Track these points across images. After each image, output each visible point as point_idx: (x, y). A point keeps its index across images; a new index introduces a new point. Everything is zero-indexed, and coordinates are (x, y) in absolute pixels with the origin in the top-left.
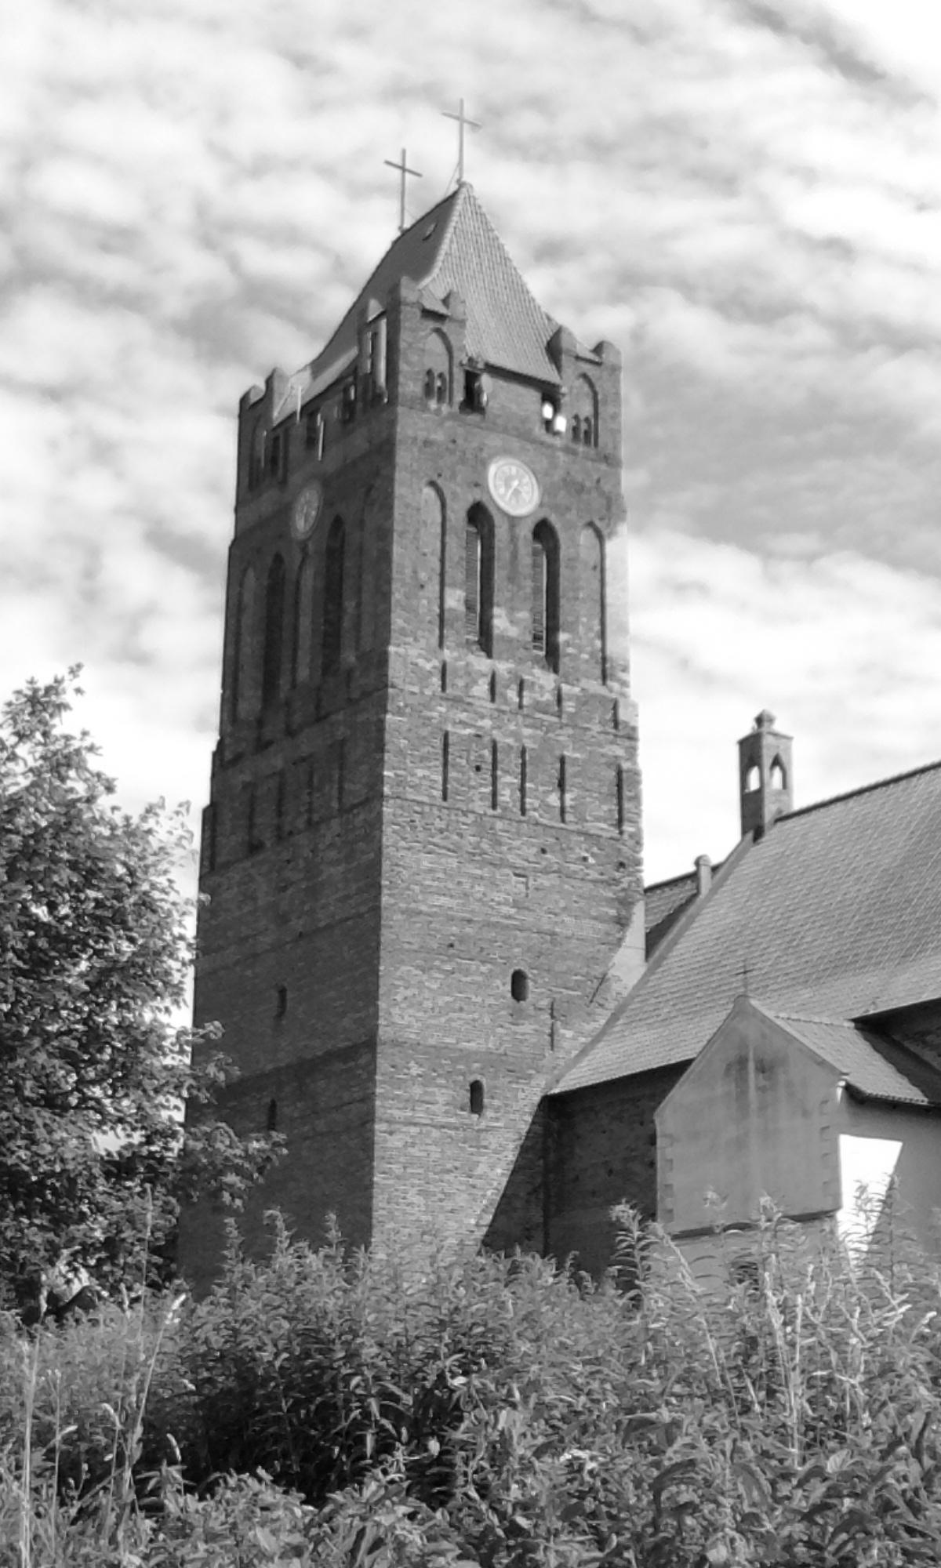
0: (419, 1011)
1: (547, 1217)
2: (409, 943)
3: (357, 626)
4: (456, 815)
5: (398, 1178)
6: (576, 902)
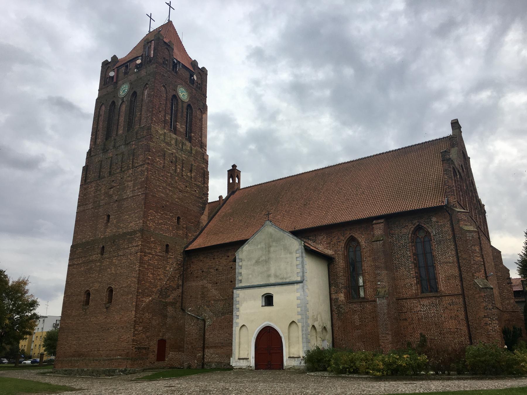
0: (154, 223)
1: (183, 283)
2: (153, 204)
3: (140, 120)
4: (166, 173)
5: (146, 269)
6: (193, 201)
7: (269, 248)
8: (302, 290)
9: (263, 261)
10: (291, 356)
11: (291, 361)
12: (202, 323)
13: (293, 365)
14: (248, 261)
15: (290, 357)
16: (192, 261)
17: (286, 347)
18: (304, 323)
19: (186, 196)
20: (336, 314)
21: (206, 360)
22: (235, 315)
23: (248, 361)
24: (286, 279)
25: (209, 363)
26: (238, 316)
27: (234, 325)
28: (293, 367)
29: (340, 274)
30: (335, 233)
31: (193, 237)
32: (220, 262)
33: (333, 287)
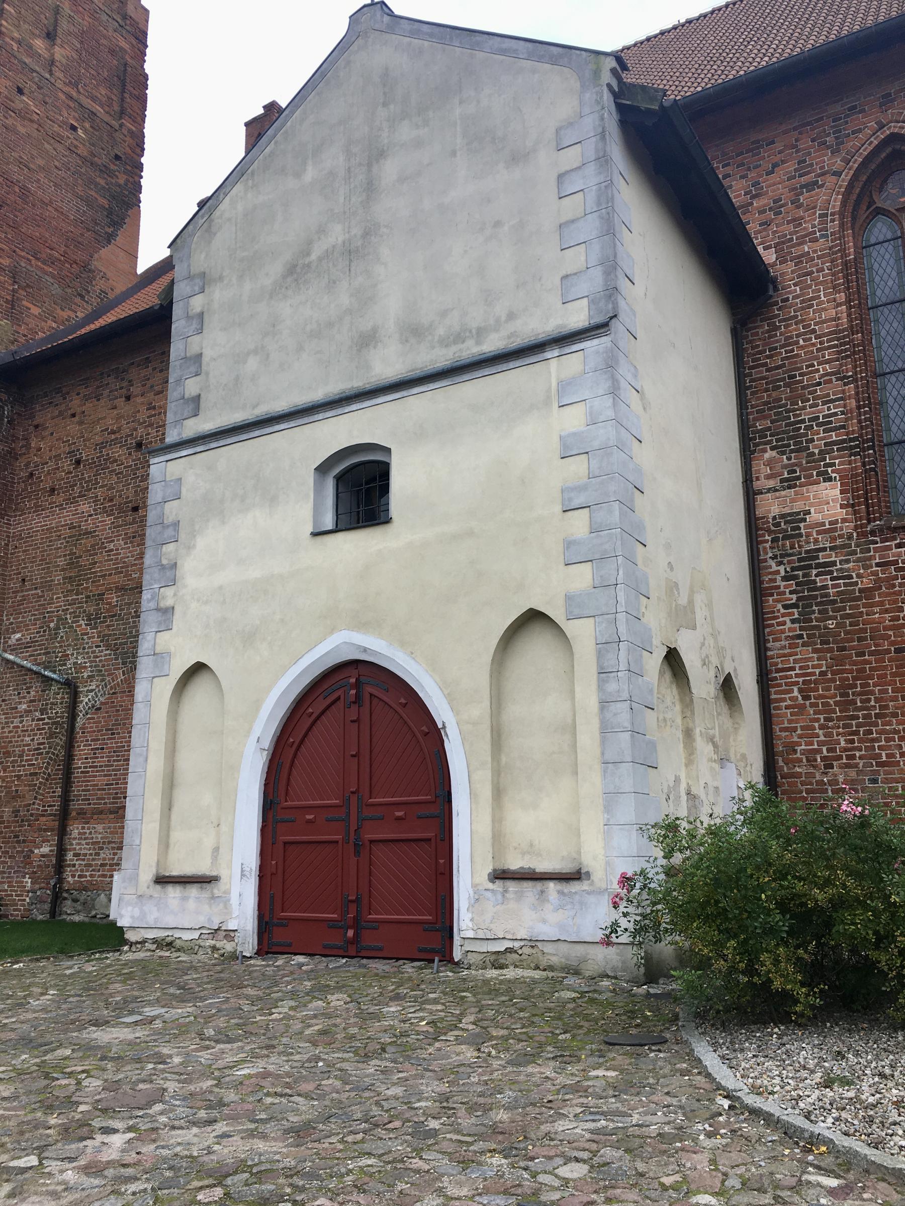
7: (370, 165)
8: (604, 386)
9: (327, 255)
10: (515, 863)
11: (512, 905)
12: (63, 698)
13: (522, 934)
14: (241, 278)
15: (501, 875)
16: (35, 423)
17: (473, 795)
18: (621, 617)
19: (16, 133)
20: (785, 607)
21: (73, 876)
22: (152, 605)
23: (213, 898)
24: (480, 333)
25: (85, 889)
26: (168, 612)
27: (145, 667)
28: (527, 950)
29: (818, 371)
30: (779, 146)
31: (54, 325)
32: (154, 408)
33: (769, 454)
